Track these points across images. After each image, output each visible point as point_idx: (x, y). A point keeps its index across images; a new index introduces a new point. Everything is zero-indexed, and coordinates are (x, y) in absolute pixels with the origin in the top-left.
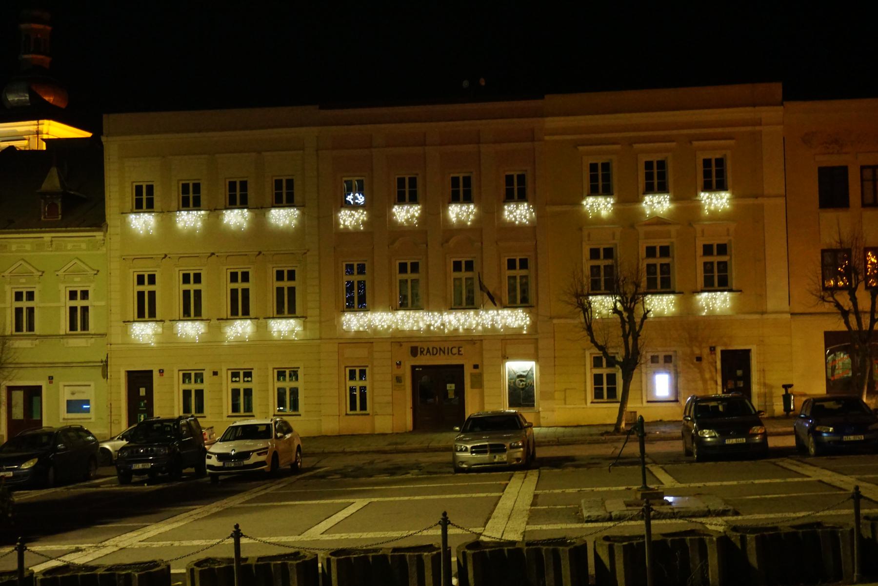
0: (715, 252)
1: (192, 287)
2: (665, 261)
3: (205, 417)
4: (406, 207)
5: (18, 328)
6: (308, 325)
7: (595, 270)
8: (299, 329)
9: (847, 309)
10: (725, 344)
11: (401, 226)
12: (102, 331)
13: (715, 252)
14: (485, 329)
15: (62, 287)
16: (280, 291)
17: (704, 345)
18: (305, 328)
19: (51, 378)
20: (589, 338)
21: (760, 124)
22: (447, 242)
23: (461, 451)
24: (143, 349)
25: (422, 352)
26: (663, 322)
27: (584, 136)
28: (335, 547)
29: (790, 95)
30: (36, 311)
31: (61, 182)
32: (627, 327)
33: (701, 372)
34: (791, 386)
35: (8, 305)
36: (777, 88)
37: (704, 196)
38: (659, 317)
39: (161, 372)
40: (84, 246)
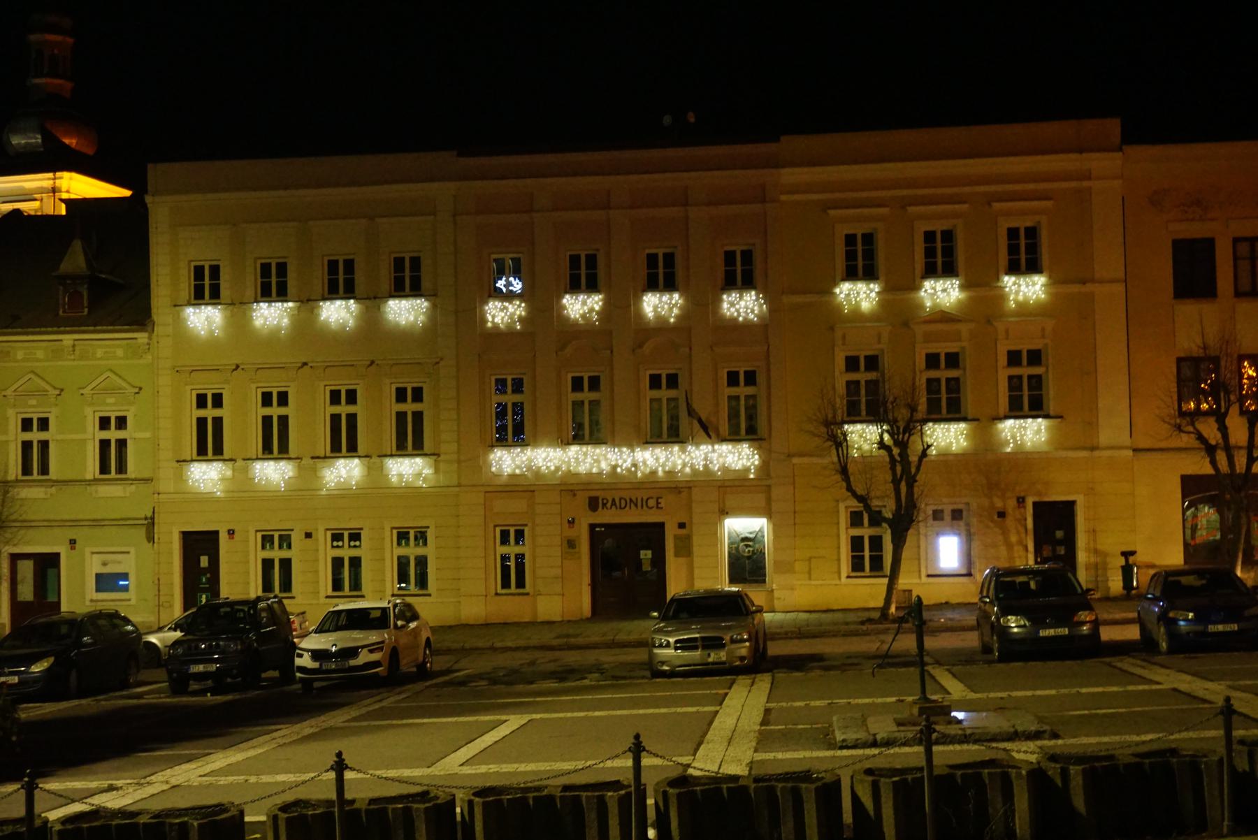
0: (1025, 361)
1: (275, 411)
2: (953, 373)
3: (293, 598)
4: (581, 297)
5: (26, 470)
6: (442, 466)
7: (853, 386)
8: (428, 471)
9: (1213, 442)
10: (1039, 494)
11: (575, 324)
12: (146, 475)
13: (1025, 361)
14: (695, 472)
15: (89, 411)
16: (401, 416)
17: (1009, 494)
18: (437, 471)
19: (73, 542)
20: (844, 484)
21: (1089, 178)
22: (640, 346)
23: (661, 646)
24: (204, 500)
25: (604, 505)
26: (949, 461)
27: (837, 195)
28: (480, 784)
29: (1131, 136)
30: (52, 446)
31: (88, 261)
32: (899, 469)
33: (1005, 533)
34: (1133, 553)
35: (11, 437)
36: (1113, 127)
37: (1009, 281)
38: (945, 455)
39: (231, 533)
40: (120, 352)
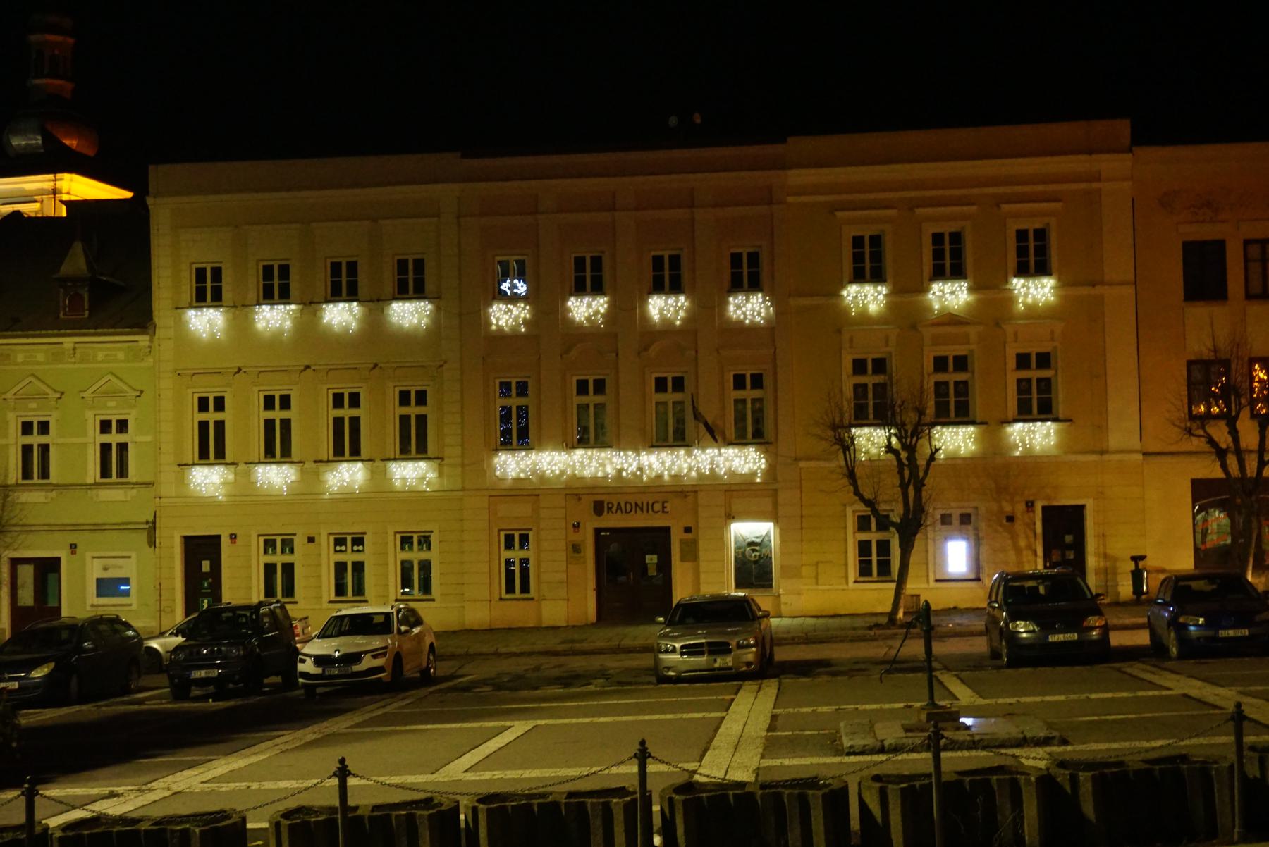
0: (1034, 364)
1: (277, 415)
2: (961, 377)
3: (296, 603)
4: (586, 300)
5: (27, 474)
6: (446, 470)
7: (860, 390)
8: (431, 475)
9: (1224, 446)
10: (1048, 498)
11: (580, 326)
12: (147, 479)
13: (1034, 364)
14: (701, 476)
15: (89, 415)
16: (404, 420)
17: (1017, 498)
18: (441, 474)
19: (73, 547)
20: (852, 488)
21: (1099, 180)
22: (646, 349)
23: (667, 651)
24: (206, 505)
25: (609, 509)
26: (958, 465)
27: (845, 197)
28: (485, 790)
29: (1141, 137)
30: (52, 449)
31: (89, 263)
32: (907, 472)
33: (1014, 537)
34: (1143, 558)
36: (1123, 128)
37: (1017, 283)
38: (953, 459)
39: (233, 537)
40: (121, 355)
